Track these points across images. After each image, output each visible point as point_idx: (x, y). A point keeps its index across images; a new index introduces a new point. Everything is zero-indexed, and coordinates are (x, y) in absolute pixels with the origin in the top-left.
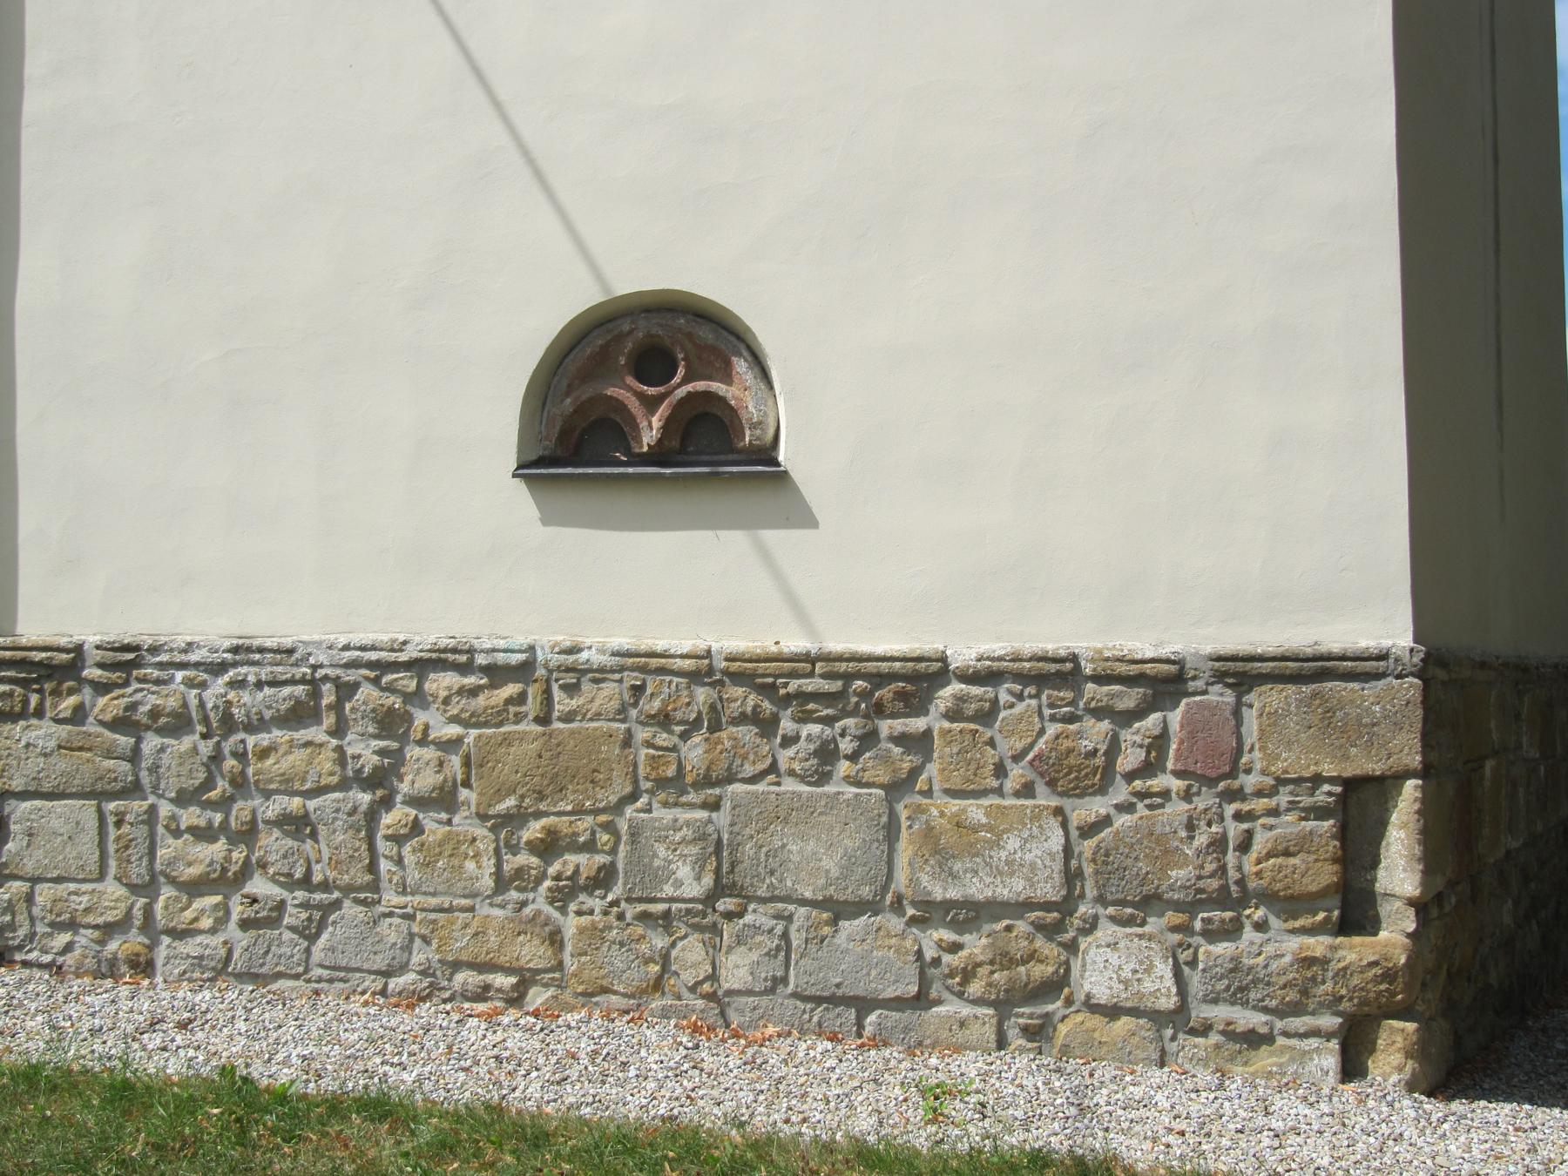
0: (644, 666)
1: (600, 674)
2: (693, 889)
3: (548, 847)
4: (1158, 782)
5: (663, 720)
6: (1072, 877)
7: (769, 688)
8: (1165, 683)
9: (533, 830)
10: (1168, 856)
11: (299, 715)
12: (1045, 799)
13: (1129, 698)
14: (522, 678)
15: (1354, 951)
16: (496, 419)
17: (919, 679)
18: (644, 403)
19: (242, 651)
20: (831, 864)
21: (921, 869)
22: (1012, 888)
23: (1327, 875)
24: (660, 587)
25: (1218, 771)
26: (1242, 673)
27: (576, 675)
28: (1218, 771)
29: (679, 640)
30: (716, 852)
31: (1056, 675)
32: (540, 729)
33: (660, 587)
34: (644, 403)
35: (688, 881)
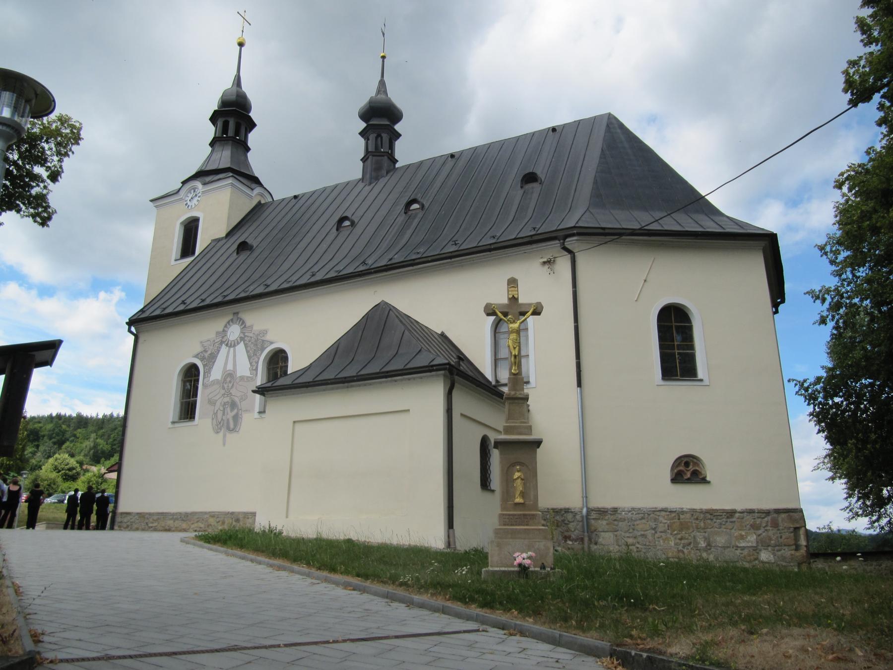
0: (693, 511)
1: (686, 512)
2: (704, 545)
3: (681, 539)
4: (768, 528)
5: (697, 519)
6: (757, 542)
7: (711, 514)
8: (767, 513)
9: (679, 536)
10: (771, 539)
11: (643, 518)
12: (752, 531)
13: (763, 515)
14: (676, 514)
15: (798, 554)
16: (667, 475)
17: (731, 513)
18: (687, 471)
19: (633, 509)
20: (723, 541)
21: (71, 131)
22: (750, 544)
23: (793, 542)
24: (690, 498)
25: (775, 525)
26: (778, 511)
27: (683, 512)
28: (775, 525)
29: (697, 506)
30: (706, 539)
31: (751, 512)
32: (189, 260)
33: (690, 498)
34: (687, 471)
35: (703, 544)
